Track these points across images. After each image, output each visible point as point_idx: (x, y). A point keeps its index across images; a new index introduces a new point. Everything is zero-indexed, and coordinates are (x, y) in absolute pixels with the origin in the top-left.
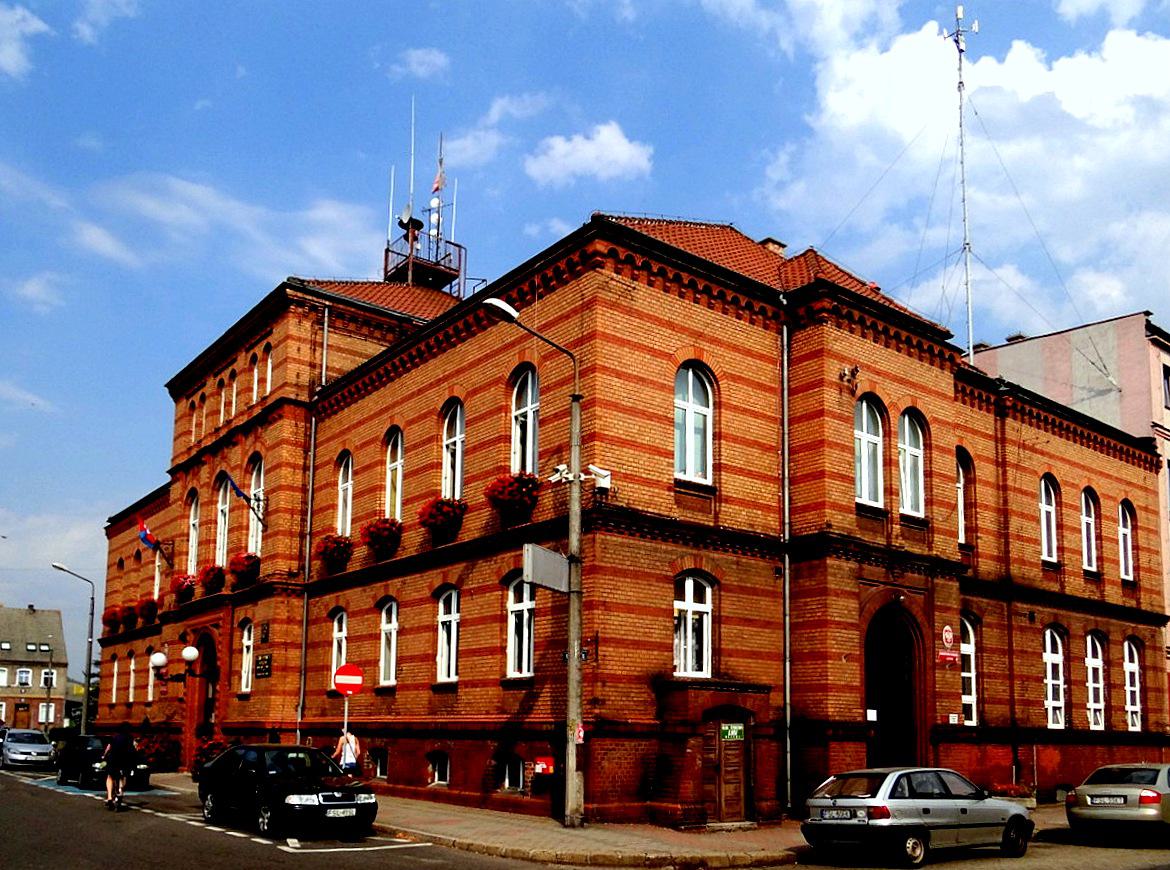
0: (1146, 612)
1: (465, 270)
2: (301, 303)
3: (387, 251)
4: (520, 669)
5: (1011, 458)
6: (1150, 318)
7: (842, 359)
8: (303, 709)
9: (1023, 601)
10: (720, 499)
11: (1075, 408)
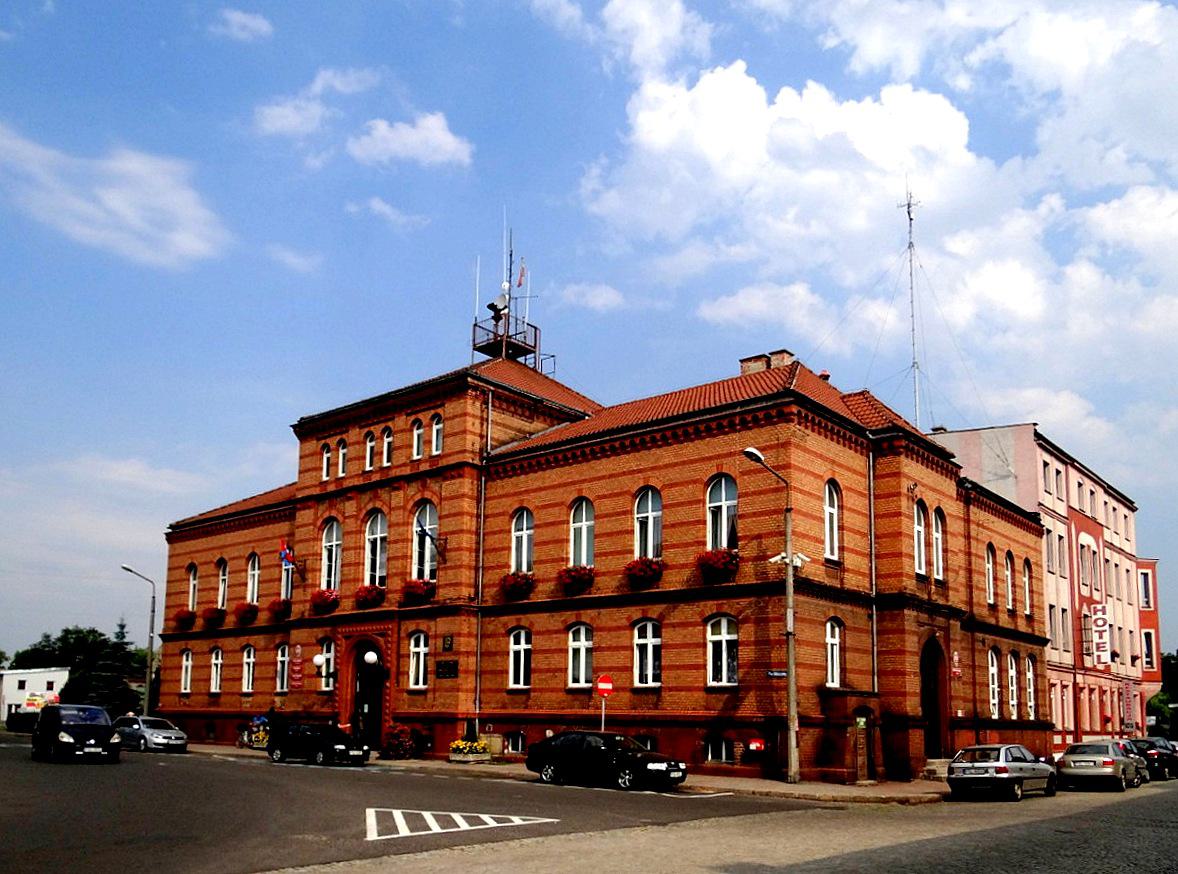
0: (1037, 637)
2: (476, 388)
3: (475, 325)
5: (973, 533)
6: (1037, 427)
7: (908, 478)
8: (480, 703)
9: (981, 632)
10: (844, 570)
11: (984, 486)
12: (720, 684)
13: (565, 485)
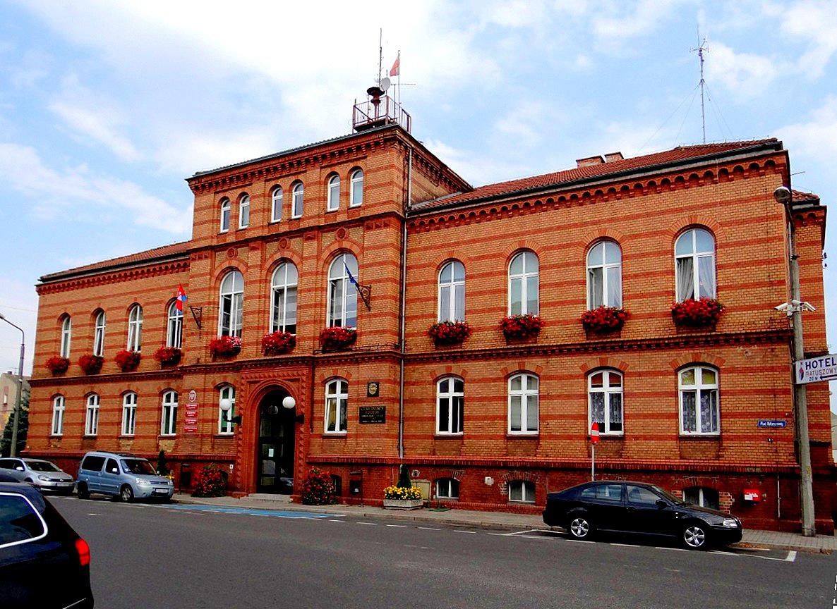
1: (384, 203)
2: (401, 143)
3: (355, 106)
4: (127, 432)
12: (693, 433)
13: (504, 237)
